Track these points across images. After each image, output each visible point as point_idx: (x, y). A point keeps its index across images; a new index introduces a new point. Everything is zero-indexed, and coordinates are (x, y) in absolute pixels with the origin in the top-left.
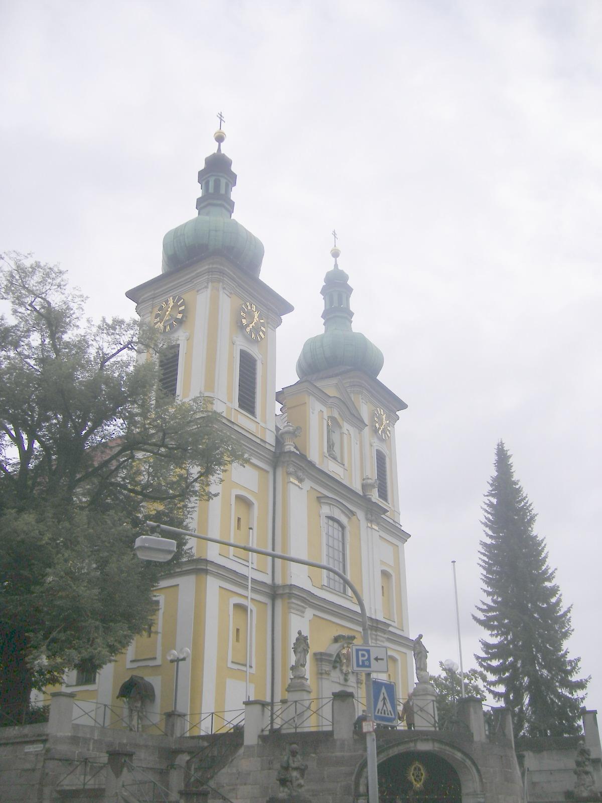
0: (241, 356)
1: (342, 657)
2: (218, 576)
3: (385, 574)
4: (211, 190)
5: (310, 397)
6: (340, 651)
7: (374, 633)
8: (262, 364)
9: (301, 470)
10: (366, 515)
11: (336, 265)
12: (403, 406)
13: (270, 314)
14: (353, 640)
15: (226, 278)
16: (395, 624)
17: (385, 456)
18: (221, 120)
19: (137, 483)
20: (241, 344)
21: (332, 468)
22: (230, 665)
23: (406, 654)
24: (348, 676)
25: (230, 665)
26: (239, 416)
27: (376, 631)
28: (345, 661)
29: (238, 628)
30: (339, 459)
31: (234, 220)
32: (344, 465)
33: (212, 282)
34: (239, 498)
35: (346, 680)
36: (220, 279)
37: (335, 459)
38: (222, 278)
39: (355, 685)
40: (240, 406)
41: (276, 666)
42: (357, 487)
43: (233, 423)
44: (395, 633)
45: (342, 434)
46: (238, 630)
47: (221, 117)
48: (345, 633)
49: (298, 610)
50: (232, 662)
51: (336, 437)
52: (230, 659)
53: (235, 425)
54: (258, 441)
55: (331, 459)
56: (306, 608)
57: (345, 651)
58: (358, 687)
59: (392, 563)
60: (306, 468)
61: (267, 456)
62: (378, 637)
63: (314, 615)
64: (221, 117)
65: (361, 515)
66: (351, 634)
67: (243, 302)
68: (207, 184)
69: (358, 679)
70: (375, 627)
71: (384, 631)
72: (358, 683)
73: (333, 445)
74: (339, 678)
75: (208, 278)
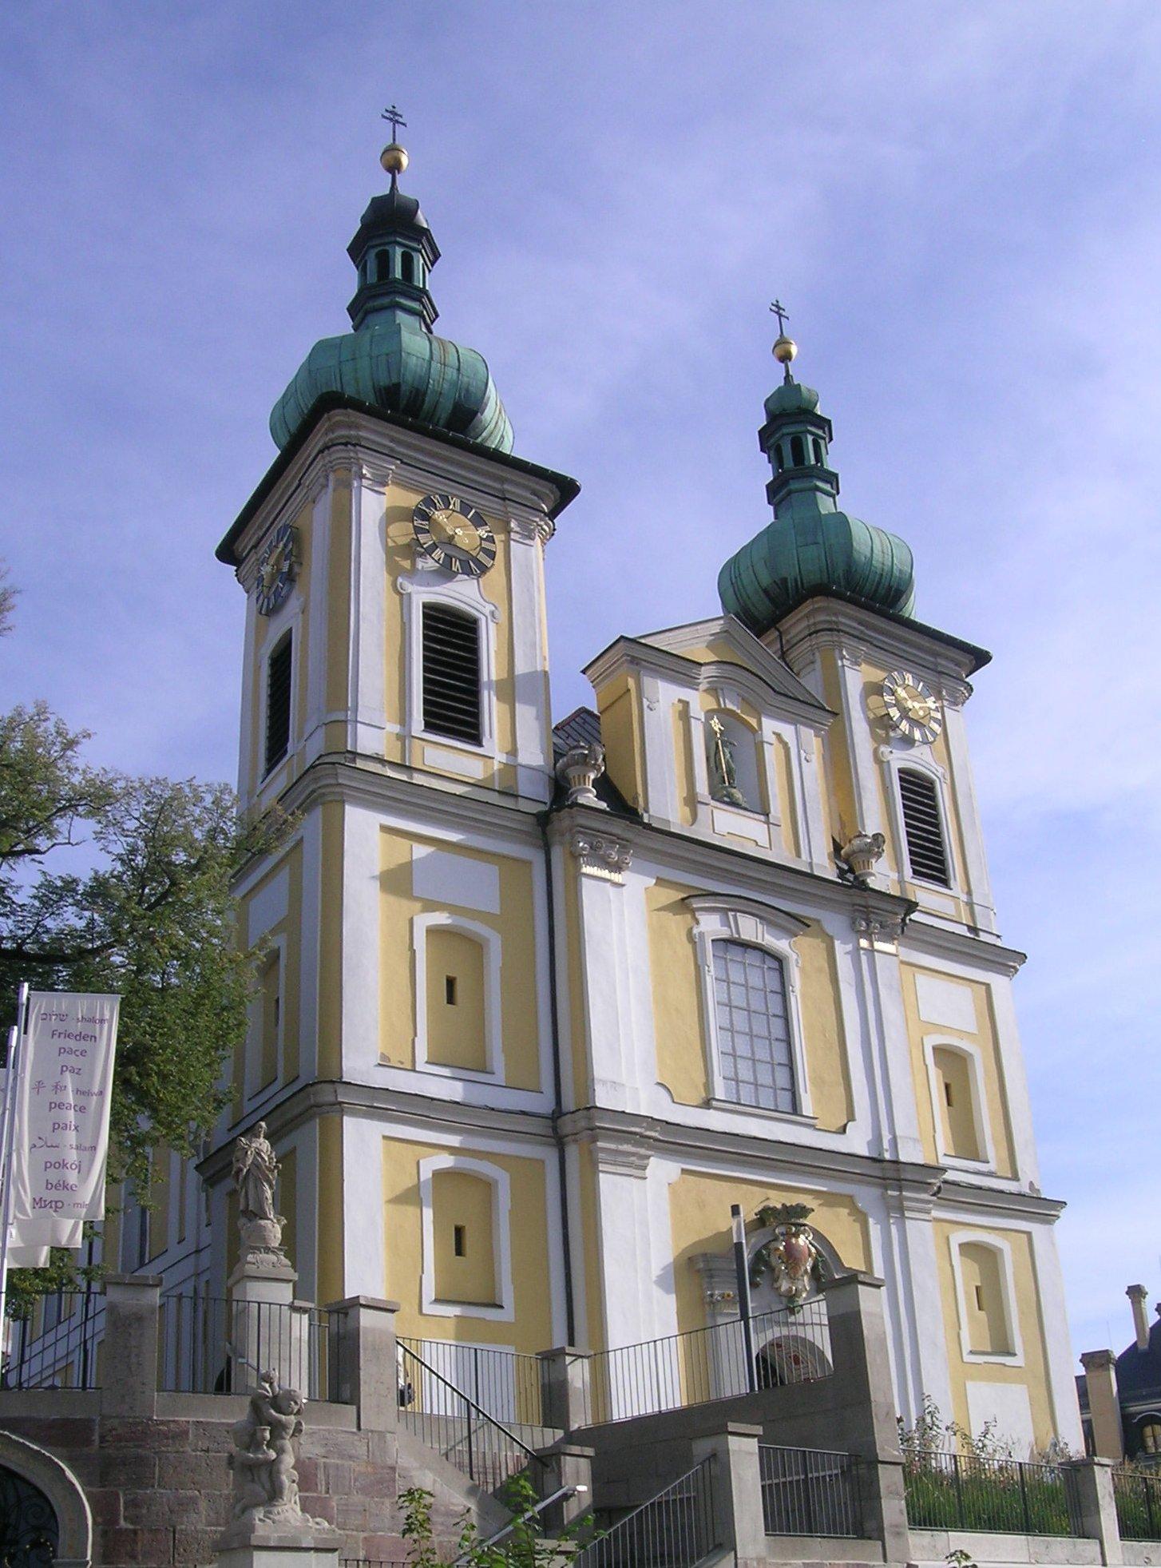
1: (774, 1261)
2: (373, 1112)
4: (372, 278)
9: (613, 842)
11: (788, 377)
12: (980, 658)
18: (780, 316)
19: (101, 936)
21: (730, 827)
22: (968, 1358)
25: (968, 1358)
26: (429, 750)
29: (460, 1223)
31: (841, 520)
37: (734, 804)
40: (429, 727)
42: (827, 869)
44: (1002, 1192)
47: (778, 310)
48: (777, 1200)
49: (920, 1211)
50: (971, 1352)
52: (967, 1346)
53: (416, 775)
56: (648, 1157)
60: (628, 835)
62: (906, 1204)
63: (385, 1137)
64: (778, 310)
66: (793, 1200)
67: (885, 675)
71: (923, 1186)
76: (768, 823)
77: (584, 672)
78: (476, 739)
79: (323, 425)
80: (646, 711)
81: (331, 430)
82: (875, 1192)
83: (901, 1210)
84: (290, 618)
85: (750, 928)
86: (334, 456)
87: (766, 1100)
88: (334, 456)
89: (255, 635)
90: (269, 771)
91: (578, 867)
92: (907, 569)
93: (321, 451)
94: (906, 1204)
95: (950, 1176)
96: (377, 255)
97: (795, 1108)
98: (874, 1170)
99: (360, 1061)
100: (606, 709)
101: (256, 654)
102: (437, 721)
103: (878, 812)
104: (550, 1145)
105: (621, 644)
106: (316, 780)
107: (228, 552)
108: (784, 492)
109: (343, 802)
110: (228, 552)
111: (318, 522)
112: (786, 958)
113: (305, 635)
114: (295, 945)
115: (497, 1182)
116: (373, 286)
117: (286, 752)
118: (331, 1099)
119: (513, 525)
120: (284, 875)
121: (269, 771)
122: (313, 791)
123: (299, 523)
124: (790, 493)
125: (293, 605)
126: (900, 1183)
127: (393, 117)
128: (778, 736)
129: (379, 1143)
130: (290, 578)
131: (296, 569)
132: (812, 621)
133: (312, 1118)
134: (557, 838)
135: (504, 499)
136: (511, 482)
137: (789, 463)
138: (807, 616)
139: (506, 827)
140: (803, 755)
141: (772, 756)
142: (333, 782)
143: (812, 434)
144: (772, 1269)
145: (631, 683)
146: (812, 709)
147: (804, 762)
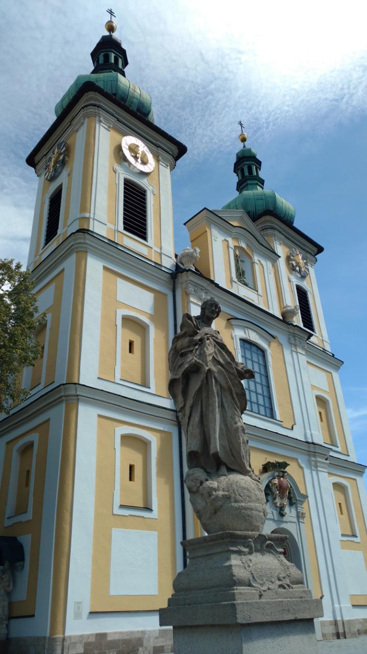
0: (297, 289)
1: (274, 489)
3: (321, 401)
5: (212, 226)
6: (270, 482)
7: (313, 459)
8: (154, 194)
9: (202, 290)
10: (289, 339)
13: (100, 112)
14: (285, 468)
15: (101, 111)
16: (339, 449)
17: (145, 191)
18: (242, 126)
20: (295, 281)
22: (117, 511)
23: (355, 480)
24: (283, 510)
25: (117, 511)
26: (125, 239)
27: (315, 456)
28: (278, 492)
29: (132, 463)
30: (251, 285)
32: (257, 291)
33: (88, 118)
34: (129, 321)
35: (282, 515)
36: (96, 112)
37: (246, 284)
38: (97, 111)
39: (295, 520)
40: (125, 229)
41: (316, 512)
43: (117, 244)
45: (253, 263)
46: (131, 468)
48: (273, 460)
51: (246, 267)
52: (117, 502)
54: (322, 350)
55: (242, 285)
57: (276, 481)
58: (299, 522)
59: (327, 389)
61: (160, 277)
63: (99, 416)
65: (282, 338)
68: (242, 171)
69: (298, 513)
70: (75, 396)
72: (298, 517)
73: (243, 272)
74: (273, 513)
75: (84, 114)
76: (258, 295)
77: (185, 224)
78: (145, 238)
79: (85, 98)
80: (213, 241)
81: (87, 100)
82: (306, 457)
83: (316, 467)
84: (63, 179)
85: (254, 337)
86: (89, 111)
87: (262, 412)
88: (89, 111)
89: (44, 190)
90: (46, 244)
91: (188, 299)
92: (293, 214)
93: (83, 108)
94: (318, 464)
95: (332, 454)
96: (104, 55)
97: (272, 416)
98: (305, 447)
99: (89, 373)
100: (194, 240)
101: (42, 199)
102: (129, 226)
103: (292, 301)
104: (174, 425)
105: (205, 211)
106: (75, 240)
107: (31, 161)
108: (245, 184)
109: (87, 252)
110: (31, 161)
111: (78, 141)
112: (266, 350)
113: (69, 188)
114: (57, 319)
115: (151, 442)
116: (102, 65)
117: (57, 233)
118: (73, 393)
119: (160, 158)
120: (52, 287)
121: (46, 244)
122: (72, 246)
123: (68, 142)
124: (247, 185)
125: (65, 173)
126: (315, 454)
127: (111, 12)
128: (259, 261)
129: (96, 418)
130: (63, 163)
131: (67, 159)
132: (263, 225)
133: (62, 401)
134: (180, 285)
135: (158, 147)
136: (159, 141)
137: (247, 174)
138: (262, 223)
139: (160, 278)
140: (269, 271)
141: (257, 268)
142: (83, 241)
143: (255, 165)
144: (273, 494)
145: (207, 229)
146: (270, 252)
147: (269, 274)
